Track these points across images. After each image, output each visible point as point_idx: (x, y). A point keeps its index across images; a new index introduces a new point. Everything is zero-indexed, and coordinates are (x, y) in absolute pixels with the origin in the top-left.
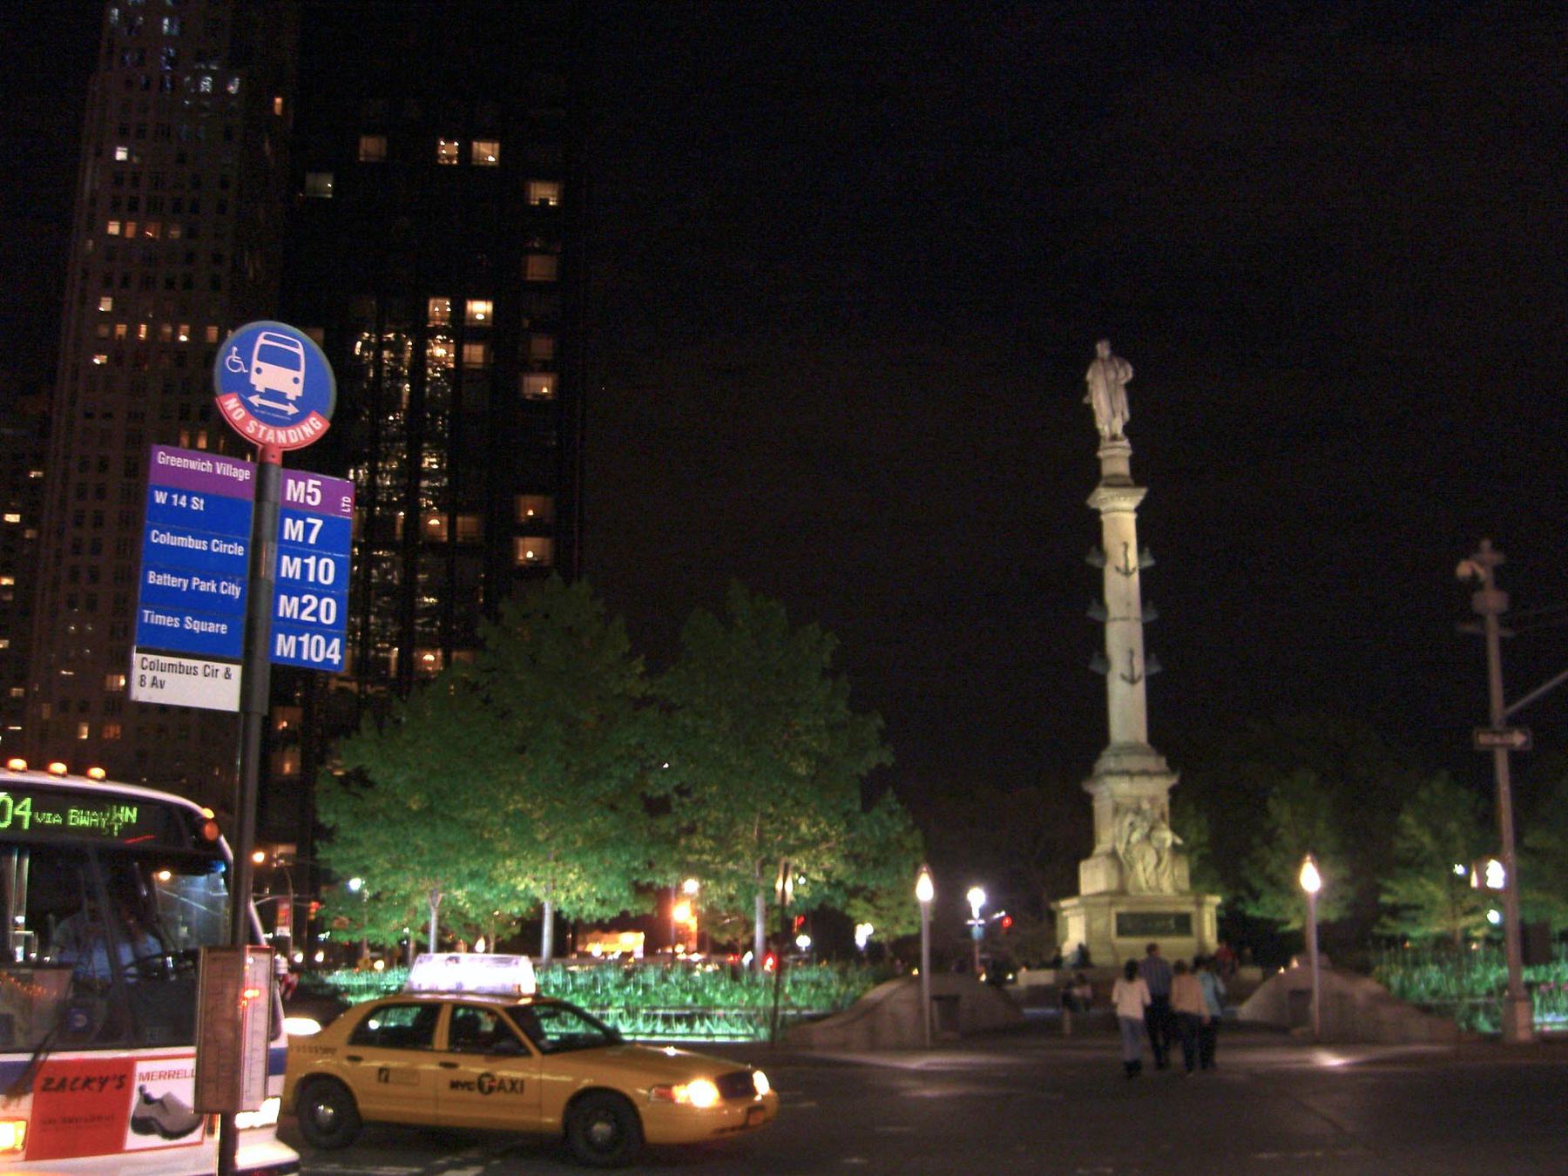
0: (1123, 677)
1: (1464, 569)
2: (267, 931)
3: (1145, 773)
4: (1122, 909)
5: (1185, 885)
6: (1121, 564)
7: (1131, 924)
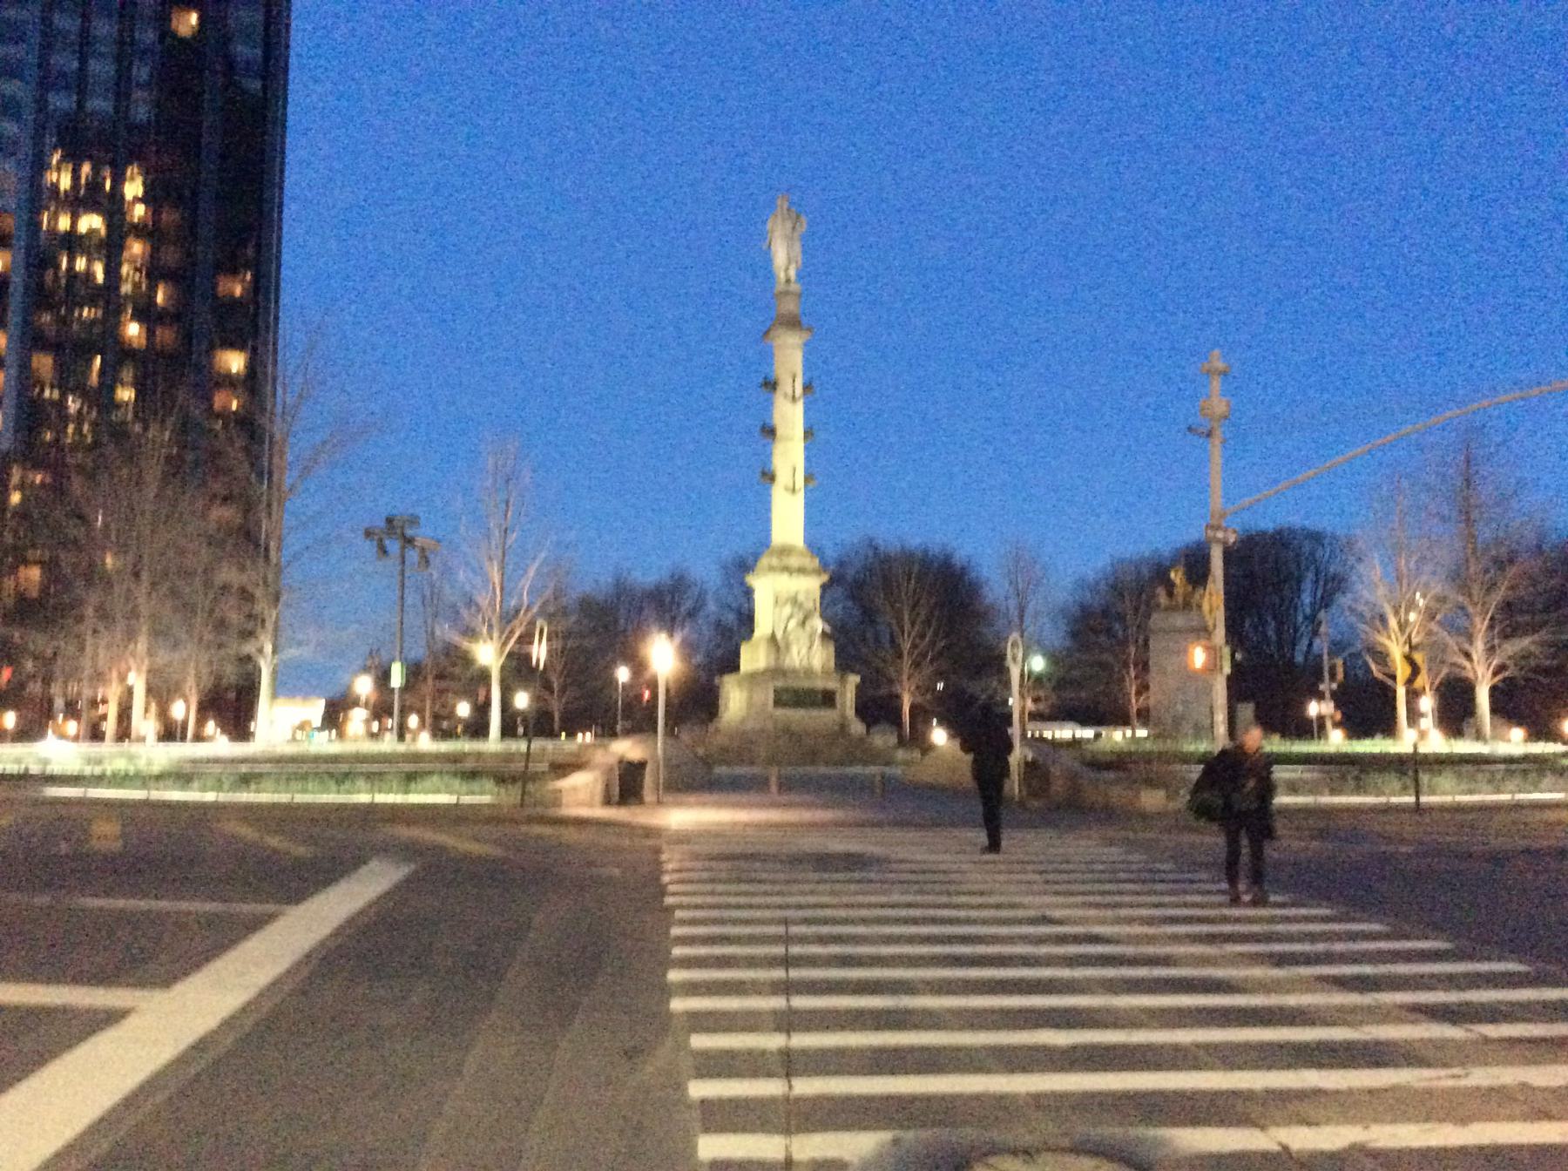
0: (786, 489)
1: (854, 679)
3: (802, 571)
4: (780, 684)
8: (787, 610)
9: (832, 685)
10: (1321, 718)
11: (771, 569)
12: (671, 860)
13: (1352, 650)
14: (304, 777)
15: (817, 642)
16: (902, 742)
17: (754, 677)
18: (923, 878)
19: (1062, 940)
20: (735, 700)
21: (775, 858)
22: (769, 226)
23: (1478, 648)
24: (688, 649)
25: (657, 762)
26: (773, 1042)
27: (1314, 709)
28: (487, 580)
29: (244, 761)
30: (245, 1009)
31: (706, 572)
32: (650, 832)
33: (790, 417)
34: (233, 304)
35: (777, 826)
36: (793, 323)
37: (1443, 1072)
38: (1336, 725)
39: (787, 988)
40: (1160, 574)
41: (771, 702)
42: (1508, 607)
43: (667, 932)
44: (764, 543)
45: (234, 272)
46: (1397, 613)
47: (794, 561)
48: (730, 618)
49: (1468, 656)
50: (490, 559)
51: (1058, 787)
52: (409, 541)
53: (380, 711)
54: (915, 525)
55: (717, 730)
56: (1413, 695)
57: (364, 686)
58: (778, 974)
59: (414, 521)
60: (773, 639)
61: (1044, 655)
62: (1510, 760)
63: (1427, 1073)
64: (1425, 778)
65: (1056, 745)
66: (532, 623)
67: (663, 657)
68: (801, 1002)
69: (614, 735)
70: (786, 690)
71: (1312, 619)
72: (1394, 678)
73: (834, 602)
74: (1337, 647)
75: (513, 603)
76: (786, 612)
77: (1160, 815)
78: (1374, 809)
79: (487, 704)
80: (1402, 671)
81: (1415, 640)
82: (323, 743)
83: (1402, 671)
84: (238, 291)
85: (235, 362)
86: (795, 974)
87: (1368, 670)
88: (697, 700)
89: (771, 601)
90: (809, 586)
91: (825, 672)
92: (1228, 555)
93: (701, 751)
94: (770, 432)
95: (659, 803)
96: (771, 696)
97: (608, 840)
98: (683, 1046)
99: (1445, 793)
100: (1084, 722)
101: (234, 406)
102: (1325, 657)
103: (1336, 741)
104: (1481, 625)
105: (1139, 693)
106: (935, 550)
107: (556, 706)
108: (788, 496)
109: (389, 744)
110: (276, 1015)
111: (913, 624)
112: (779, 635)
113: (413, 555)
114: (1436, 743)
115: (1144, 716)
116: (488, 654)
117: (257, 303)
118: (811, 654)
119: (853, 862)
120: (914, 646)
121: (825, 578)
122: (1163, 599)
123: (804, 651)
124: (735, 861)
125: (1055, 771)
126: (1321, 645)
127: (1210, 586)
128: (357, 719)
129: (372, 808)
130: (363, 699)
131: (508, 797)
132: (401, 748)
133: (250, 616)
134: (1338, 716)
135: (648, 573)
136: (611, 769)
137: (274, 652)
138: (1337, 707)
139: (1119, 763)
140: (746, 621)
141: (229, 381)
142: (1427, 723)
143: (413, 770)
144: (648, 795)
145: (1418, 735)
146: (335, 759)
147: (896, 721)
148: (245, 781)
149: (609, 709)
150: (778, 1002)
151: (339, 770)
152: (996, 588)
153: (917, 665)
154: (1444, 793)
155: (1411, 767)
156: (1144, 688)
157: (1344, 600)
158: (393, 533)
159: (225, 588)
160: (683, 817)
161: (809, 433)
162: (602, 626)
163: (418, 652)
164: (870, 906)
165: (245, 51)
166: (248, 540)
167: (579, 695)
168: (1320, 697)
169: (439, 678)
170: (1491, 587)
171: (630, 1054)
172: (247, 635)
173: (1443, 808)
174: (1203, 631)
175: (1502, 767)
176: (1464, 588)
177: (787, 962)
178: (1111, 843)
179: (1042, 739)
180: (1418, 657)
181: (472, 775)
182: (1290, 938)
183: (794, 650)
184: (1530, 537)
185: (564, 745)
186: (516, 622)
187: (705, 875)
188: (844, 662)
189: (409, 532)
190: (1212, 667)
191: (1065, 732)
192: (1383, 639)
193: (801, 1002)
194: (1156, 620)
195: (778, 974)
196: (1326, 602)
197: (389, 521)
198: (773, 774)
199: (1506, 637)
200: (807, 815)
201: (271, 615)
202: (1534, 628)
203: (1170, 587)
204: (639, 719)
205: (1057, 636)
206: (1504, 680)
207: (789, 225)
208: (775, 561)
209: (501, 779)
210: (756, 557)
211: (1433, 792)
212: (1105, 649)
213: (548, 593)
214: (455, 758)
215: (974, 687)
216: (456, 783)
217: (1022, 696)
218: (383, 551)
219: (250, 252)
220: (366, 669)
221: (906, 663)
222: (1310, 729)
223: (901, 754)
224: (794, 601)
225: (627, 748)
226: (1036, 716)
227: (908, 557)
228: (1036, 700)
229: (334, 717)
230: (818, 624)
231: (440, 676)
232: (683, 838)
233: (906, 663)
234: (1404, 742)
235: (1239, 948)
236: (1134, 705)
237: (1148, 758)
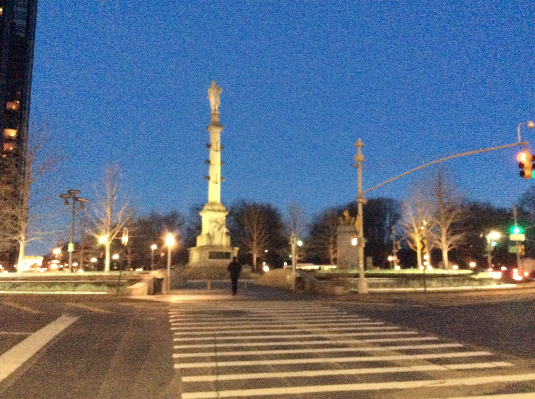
0: (214, 182)
1: (237, 249)
2: (393, 267)
3: (219, 211)
4: (211, 250)
5: (229, 244)
6: (215, 148)
7: (212, 255)
8: (214, 224)
9: (229, 251)
10: (393, 262)
11: (208, 210)
12: (173, 314)
13: (403, 239)
14: (37, 285)
15: (224, 236)
16: (253, 271)
17: (202, 248)
18: (261, 318)
19: (312, 339)
20: (195, 256)
21: (208, 313)
22: (209, 90)
23: (443, 239)
24: (179, 238)
25: (167, 278)
26: (212, 378)
27: (390, 258)
28: (105, 214)
29: (13, 279)
30: (18, 370)
31: (185, 211)
32: (165, 304)
33: (216, 157)
34: (10, 112)
35: (209, 301)
36: (217, 125)
37: (438, 381)
38: (398, 264)
39: (215, 359)
40: (340, 213)
41: (207, 258)
42: (452, 225)
43: (171, 340)
44: (206, 201)
45: (12, 100)
46: (417, 226)
47: (216, 207)
48: (193, 227)
49: (440, 241)
50: (107, 205)
51: (307, 287)
52: (76, 199)
53: (64, 260)
54: (257, 196)
55: (189, 267)
56: (422, 254)
57: (57, 252)
58: (212, 354)
59: (79, 191)
60: (208, 234)
61: (302, 241)
62: (455, 276)
63: (433, 382)
64: (427, 282)
65: (305, 271)
66: (122, 230)
67: (170, 241)
68: (221, 364)
69: (150, 269)
70: (213, 252)
71: (390, 228)
72: (416, 248)
73: (230, 222)
74: (398, 238)
75: (115, 222)
76: (213, 225)
77: (343, 295)
78: (411, 293)
79: (104, 258)
80: (419, 246)
81: (424, 236)
82: (42, 272)
83: (419, 246)
84: (14, 107)
85: (12, 133)
86: (219, 354)
87: (408, 246)
88: (181, 256)
89: (208, 221)
90: (222, 216)
91: (228, 247)
92: (365, 208)
93: (182, 274)
94: (208, 162)
95: (168, 294)
96: (208, 254)
97: (150, 307)
98: (180, 380)
99: (434, 287)
100: (316, 262)
101: (11, 149)
102: (394, 241)
103: (397, 269)
104: (444, 231)
105: (334, 253)
106: (265, 204)
107: (129, 258)
108: (214, 184)
109: (67, 273)
110: (28, 374)
111: (257, 229)
112: (211, 233)
113: (78, 204)
114: (431, 270)
115: (335, 261)
116: (104, 240)
117: (21, 113)
118: (222, 240)
119: (238, 313)
120: (258, 237)
121: (227, 213)
122: (342, 222)
123: (220, 239)
124: (196, 314)
125: (307, 280)
126: (392, 237)
127: (358, 217)
128: (54, 265)
129: (61, 295)
130: (56, 257)
131: (113, 291)
132: (72, 274)
133: (16, 226)
134: (398, 261)
135: (163, 211)
136: (151, 281)
137: (26, 239)
138: (398, 258)
139: (328, 277)
140: (199, 228)
141: (10, 140)
142: (427, 263)
143: (77, 282)
144: (164, 291)
145: (425, 267)
146: (47, 278)
147: (251, 264)
148: (14, 286)
149: (149, 260)
150: (213, 364)
151: (51, 282)
152: (285, 216)
153: (258, 244)
154: (432, 287)
155: (423, 278)
156: (335, 252)
157: (400, 222)
158: (71, 196)
159: (7, 215)
160: (176, 298)
161: (222, 163)
162: (147, 230)
163: (78, 238)
164: (245, 329)
165: (20, 22)
166: (16, 197)
167: (138, 256)
168: (393, 255)
169: (86, 248)
170: (447, 218)
171: (161, 384)
172: (15, 233)
173: (433, 292)
174: (356, 233)
175: (453, 278)
176: (439, 218)
177: (216, 350)
178: (324, 305)
179: (301, 270)
180: (425, 242)
181: (98, 284)
182: (385, 337)
183: (216, 238)
184: (459, 202)
185: (130, 273)
186: (115, 229)
187: (195, 319)
188: (233, 244)
189: (77, 195)
190: (359, 244)
191: (309, 267)
192: (413, 235)
193: (221, 364)
194: (339, 229)
195: (212, 354)
196: (393, 223)
197: (69, 191)
198: (209, 282)
199: (453, 234)
200: (215, 297)
201: (23, 225)
202: (460, 232)
203: (344, 217)
204: (159, 262)
205: (306, 234)
206: (452, 249)
207: (216, 91)
208: (209, 207)
209: (110, 285)
210: (203, 206)
211: (429, 286)
212: (322, 239)
213: (128, 219)
214: (89, 278)
215: (278, 252)
216: (93, 287)
217: (295, 255)
218: (67, 203)
219: (19, 93)
220: (58, 246)
221: (255, 244)
222: (388, 265)
223: (253, 275)
224: (216, 222)
225: (156, 274)
226: (299, 262)
227: (255, 206)
228: (299, 256)
229: (45, 264)
230: (225, 230)
231: (86, 248)
232: (177, 306)
233: (255, 244)
234: (420, 271)
235: (368, 341)
236: (332, 257)
237: (338, 276)
